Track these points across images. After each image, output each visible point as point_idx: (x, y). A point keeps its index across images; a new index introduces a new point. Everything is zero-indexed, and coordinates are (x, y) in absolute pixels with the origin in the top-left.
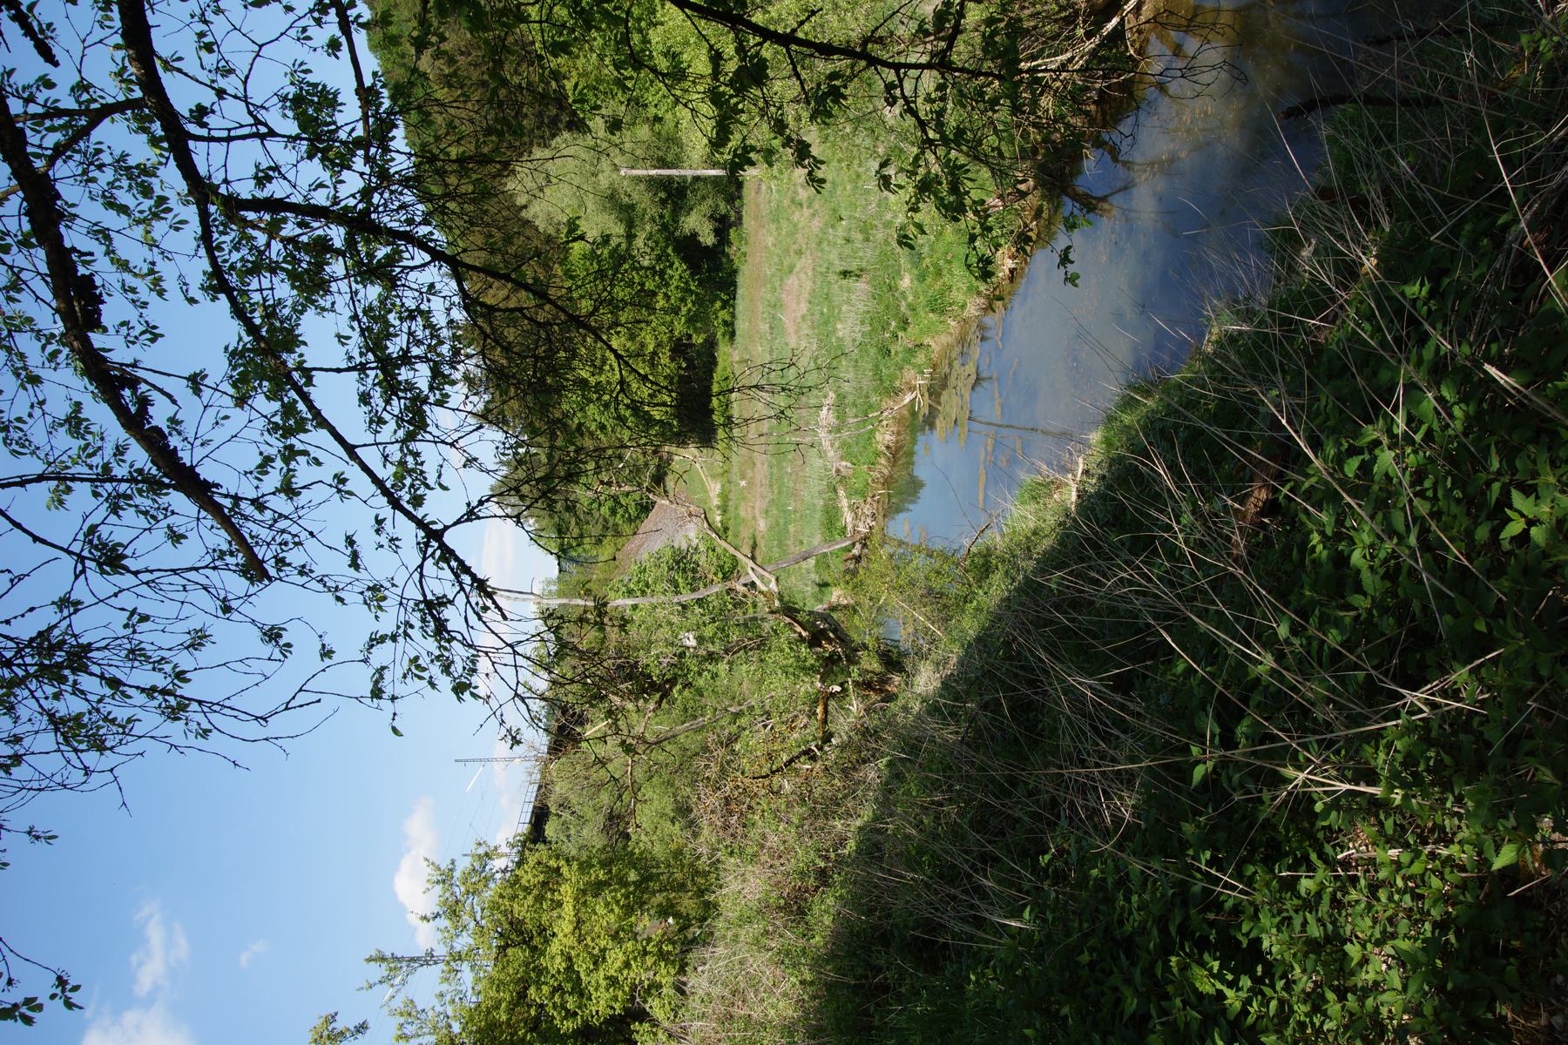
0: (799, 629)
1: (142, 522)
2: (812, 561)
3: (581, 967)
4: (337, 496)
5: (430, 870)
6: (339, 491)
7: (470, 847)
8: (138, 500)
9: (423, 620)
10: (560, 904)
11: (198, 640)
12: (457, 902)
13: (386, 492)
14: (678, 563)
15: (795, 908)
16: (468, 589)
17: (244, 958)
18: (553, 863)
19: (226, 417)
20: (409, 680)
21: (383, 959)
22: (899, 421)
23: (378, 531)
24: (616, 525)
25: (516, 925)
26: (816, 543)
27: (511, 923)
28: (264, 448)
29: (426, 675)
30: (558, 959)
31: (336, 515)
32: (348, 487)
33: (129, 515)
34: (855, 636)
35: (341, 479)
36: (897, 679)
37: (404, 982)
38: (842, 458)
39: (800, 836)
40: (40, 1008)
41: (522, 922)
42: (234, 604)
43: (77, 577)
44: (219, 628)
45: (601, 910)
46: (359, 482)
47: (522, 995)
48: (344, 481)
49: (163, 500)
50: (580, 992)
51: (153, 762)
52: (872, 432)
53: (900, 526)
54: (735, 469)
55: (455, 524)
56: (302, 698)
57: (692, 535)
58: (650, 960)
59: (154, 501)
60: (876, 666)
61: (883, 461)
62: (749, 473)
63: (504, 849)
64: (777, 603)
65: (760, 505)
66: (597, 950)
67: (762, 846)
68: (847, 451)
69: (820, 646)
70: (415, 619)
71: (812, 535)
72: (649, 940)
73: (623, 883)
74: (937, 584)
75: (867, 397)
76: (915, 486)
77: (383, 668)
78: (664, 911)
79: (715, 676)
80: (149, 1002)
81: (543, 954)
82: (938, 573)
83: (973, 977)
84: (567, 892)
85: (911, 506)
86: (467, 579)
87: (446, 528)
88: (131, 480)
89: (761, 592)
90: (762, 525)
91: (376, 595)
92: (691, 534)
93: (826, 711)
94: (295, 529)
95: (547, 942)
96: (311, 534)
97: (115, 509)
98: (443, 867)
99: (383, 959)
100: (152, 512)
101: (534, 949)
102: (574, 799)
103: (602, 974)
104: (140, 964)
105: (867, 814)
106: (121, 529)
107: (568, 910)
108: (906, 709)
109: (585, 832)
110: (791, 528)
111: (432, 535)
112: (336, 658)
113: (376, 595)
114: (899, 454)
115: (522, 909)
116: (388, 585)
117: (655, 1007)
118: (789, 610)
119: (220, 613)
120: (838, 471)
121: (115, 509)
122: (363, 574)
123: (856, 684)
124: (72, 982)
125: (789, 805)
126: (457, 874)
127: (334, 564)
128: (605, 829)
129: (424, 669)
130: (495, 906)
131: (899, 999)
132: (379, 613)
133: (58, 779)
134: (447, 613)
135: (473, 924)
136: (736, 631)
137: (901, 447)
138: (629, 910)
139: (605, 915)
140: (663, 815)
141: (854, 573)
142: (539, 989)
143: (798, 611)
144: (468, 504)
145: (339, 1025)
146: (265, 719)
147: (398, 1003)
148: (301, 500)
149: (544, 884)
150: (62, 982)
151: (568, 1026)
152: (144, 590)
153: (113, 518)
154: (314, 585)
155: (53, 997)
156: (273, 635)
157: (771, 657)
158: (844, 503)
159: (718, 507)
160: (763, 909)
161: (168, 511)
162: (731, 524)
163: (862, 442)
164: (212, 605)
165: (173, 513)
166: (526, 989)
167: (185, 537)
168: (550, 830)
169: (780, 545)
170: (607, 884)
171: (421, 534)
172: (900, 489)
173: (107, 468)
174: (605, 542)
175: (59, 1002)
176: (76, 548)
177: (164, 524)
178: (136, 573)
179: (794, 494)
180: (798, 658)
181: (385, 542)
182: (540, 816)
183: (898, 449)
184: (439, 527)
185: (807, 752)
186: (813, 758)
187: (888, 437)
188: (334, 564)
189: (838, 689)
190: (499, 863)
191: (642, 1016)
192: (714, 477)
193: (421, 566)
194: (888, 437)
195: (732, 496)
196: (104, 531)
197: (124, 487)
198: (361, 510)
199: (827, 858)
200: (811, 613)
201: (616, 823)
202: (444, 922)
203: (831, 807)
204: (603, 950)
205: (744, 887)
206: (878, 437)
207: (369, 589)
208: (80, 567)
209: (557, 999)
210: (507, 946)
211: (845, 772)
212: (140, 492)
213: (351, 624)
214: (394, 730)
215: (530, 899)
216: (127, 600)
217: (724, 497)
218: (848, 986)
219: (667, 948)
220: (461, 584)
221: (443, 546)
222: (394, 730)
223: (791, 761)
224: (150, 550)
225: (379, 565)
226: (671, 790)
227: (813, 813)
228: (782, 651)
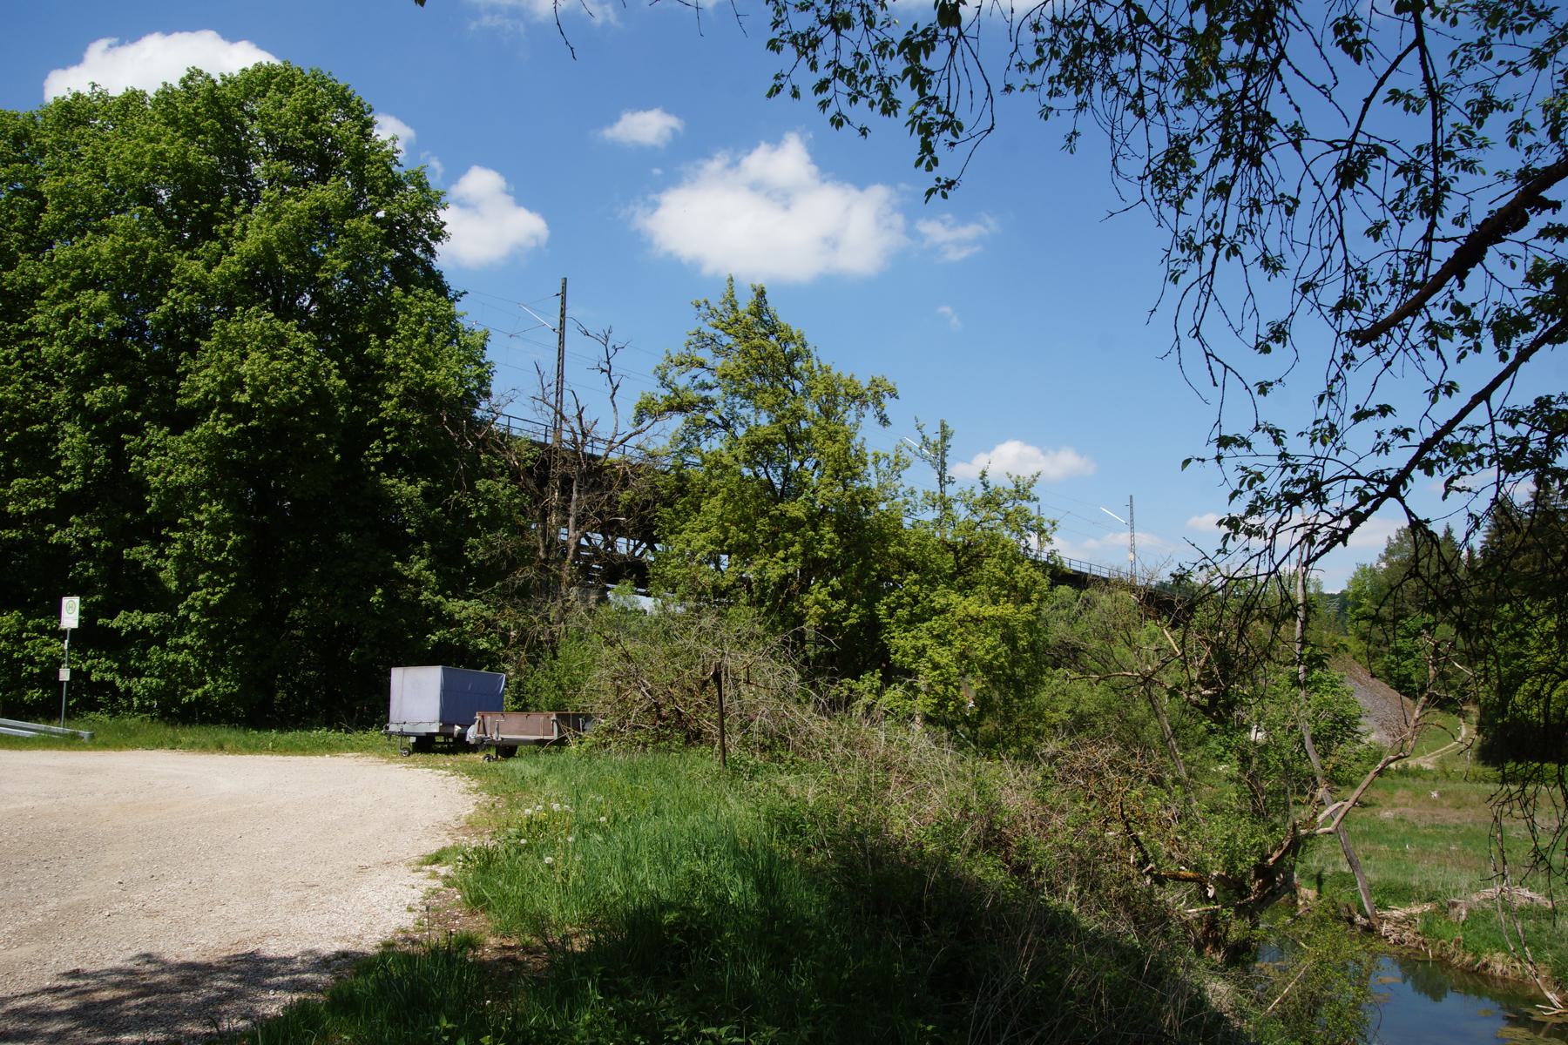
0: (1276, 855)
1: (1391, 196)
2: (1346, 869)
3: (935, 623)
4: (1431, 386)
5: (1028, 477)
6: (1437, 388)
7: (1048, 516)
8: (1415, 191)
9: (1300, 481)
10: (995, 602)
11: (1271, 264)
12: (998, 505)
13: (1438, 436)
14: (1342, 721)
15: (993, 841)
16: (1334, 525)
17: (947, 310)
18: (1035, 596)
19: (1513, 266)
20: (1240, 473)
21: (944, 438)
22: (1521, 982)
23: (1395, 431)
24: (1382, 654)
25: (976, 560)
26: (1368, 874)
27: (977, 556)
28: (1481, 307)
29: (1245, 487)
30: (943, 601)
31: (1409, 387)
32: (1442, 397)
33: (1400, 182)
34: (1267, 915)
35: (1450, 389)
36: (1218, 957)
37: (924, 458)
38: (1470, 910)
39: (1062, 848)
40: (929, 169)
41: (979, 565)
42: (1310, 295)
43: (1330, 143)
44: (1283, 284)
45: (989, 642)
46: (1447, 409)
47: (910, 566)
48: (1449, 392)
49: (1415, 214)
50: (913, 621)
51: (1147, 233)
52: (1505, 949)
53: (1389, 976)
54: (1451, 786)
55: (1406, 509)
56: (1218, 369)
57: (1373, 737)
58: (939, 688)
59: (1413, 206)
60: (1233, 936)
61: (1468, 958)
62: (1446, 803)
63: (1048, 548)
64: (1303, 832)
65: (1410, 812)
66: (946, 640)
67: (1051, 809)
68: (1478, 917)
69: (1257, 877)
70: (1302, 473)
71: (1376, 870)
72: (958, 688)
73: (1014, 663)
74: (1325, 1013)
75: (1551, 947)
76: (1436, 993)
77: (1249, 445)
78: (984, 703)
79: (1220, 758)
80: (911, 233)
81: (949, 586)
82: (1339, 1015)
83: (930, 1028)
84: (1006, 609)
85: (1409, 983)
86: (1346, 523)
87: (1401, 500)
88: (1437, 179)
89: (1315, 815)
90: (1387, 814)
91: (1328, 433)
92: (1374, 735)
93: (1187, 879)
94: (1392, 347)
95: (960, 589)
96: (1389, 364)
97: (1403, 169)
98: (1032, 490)
99: (944, 438)
100: (1402, 205)
101: (953, 577)
102: (1095, 614)
103: (929, 642)
104: (943, 222)
105: (1088, 922)
106: (1383, 180)
107: (990, 611)
108: (1189, 966)
109: (1062, 624)
110: (1383, 847)
111: (1395, 486)
112: (1259, 399)
113: (1328, 433)
114: (1477, 979)
115: (991, 567)
116: (1338, 444)
117: (894, 694)
118: (1297, 845)
119: (1300, 282)
120: (1454, 905)
121: (1403, 169)
122: (1348, 422)
123: (1215, 913)
124: (949, 193)
125: (1094, 838)
126: (1025, 504)
127: (1357, 392)
128: (1064, 645)
129: (1250, 487)
130: (994, 540)
131: (906, 945)
132: (1307, 438)
133: (1124, 150)
134: (1309, 507)
135: (977, 519)
136: (1274, 785)
137: (1486, 982)
138: (987, 668)
139: (984, 645)
140: (1077, 702)
141: (1337, 918)
142: (916, 582)
143: (1295, 854)
144: (1428, 521)
145: (887, 402)
146: (1197, 334)
147: (906, 454)
148: (1425, 351)
149: (1015, 588)
150: (950, 184)
151: (882, 610)
152: (1322, 205)
153: (1393, 168)
154: (1334, 370)
155: (938, 180)
156: (1279, 333)
157: (1245, 823)
158: (1416, 910)
159: (1405, 766)
160: (993, 808)
161: (1403, 221)
162: (1387, 779)
163: (1491, 936)
164: (1307, 273)
165: (1402, 225)
166: (916, 571)
167: (1376, 240)
168: (1064, 590)
169: (1365, 835)
170: (1014, 648)
171: (1392, 474)
172: (1430, 974)
173: (1449, 156)
174: (1364, 643)
175: (933, 184)
176: (1361, 139)
177: (1390, 217)
178: (1336, 197)
179: (1424, 852)
180: (1243, 851)
181: (1384, 438)
182: (1079, 580)
183: (1485, 978)
184: (1402, 493)
185: (1146, 860)
186: (1141, 865)
187: (1499, 967)
188: (1357, 392)
189: (1211, 894)
190: (1033, 540)
191: (887, 681)
192: (1441, 761)
193: (1358, 477)
194: (1499, 967)
195: (1419, 780)
196: (1380, 161)
197: (1430, 175)
198: (1418, 415)
199: (1039, 874)
200: (1293, 868)
201: (1069, 655)
202: (979, 492)
203: (1090, 881)
204: (950, 643)
205: (1012, 788)
206: (1499, 956)
207: (1332, 426)
208: (1340, 145)
209: (907, 599)
210: (956, 553)
211: (1124, 899)
212: (1424, 191)
213: (1294, 411)
214: (1187, 462)
215: (1002, 574)
216: (1309, 194)
217: (1418, 773)
218: (921, 893)
219: (951, 706)
220: (1340, 518)
221: (1382, 497)
222: (1187, 462)
223: (1138, 843)
224: (1361, 207)
225: (1359, 438)
226: (1102, 711)
227: (1083, 863)
228: (1252, 836)
